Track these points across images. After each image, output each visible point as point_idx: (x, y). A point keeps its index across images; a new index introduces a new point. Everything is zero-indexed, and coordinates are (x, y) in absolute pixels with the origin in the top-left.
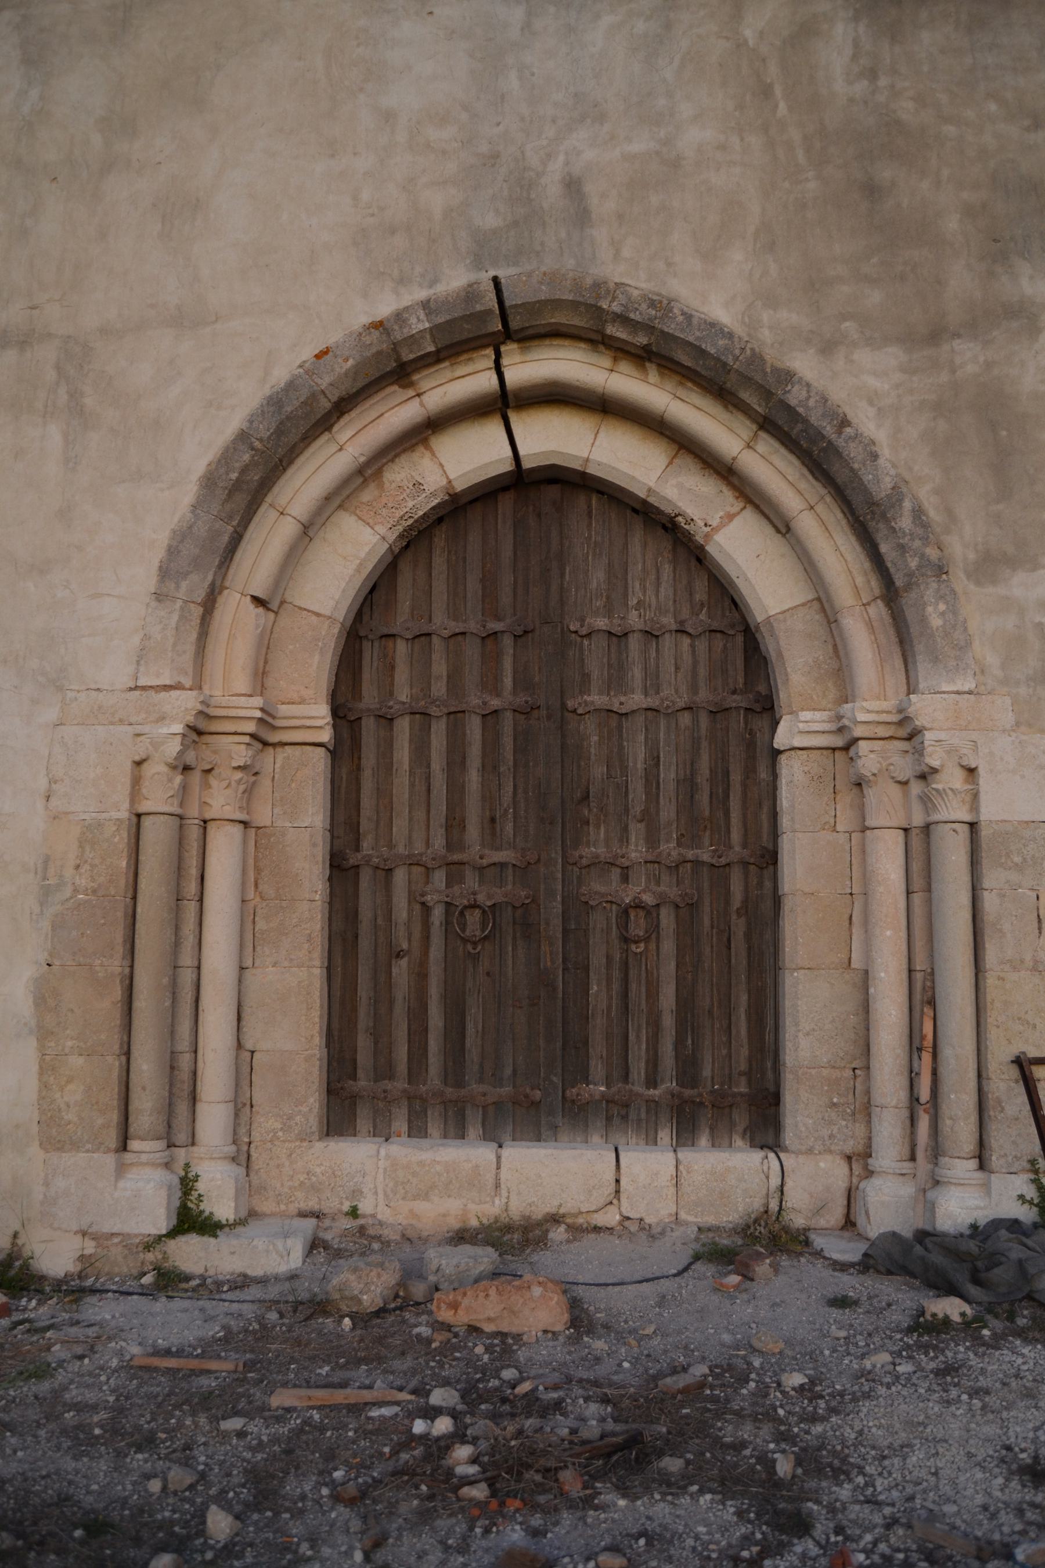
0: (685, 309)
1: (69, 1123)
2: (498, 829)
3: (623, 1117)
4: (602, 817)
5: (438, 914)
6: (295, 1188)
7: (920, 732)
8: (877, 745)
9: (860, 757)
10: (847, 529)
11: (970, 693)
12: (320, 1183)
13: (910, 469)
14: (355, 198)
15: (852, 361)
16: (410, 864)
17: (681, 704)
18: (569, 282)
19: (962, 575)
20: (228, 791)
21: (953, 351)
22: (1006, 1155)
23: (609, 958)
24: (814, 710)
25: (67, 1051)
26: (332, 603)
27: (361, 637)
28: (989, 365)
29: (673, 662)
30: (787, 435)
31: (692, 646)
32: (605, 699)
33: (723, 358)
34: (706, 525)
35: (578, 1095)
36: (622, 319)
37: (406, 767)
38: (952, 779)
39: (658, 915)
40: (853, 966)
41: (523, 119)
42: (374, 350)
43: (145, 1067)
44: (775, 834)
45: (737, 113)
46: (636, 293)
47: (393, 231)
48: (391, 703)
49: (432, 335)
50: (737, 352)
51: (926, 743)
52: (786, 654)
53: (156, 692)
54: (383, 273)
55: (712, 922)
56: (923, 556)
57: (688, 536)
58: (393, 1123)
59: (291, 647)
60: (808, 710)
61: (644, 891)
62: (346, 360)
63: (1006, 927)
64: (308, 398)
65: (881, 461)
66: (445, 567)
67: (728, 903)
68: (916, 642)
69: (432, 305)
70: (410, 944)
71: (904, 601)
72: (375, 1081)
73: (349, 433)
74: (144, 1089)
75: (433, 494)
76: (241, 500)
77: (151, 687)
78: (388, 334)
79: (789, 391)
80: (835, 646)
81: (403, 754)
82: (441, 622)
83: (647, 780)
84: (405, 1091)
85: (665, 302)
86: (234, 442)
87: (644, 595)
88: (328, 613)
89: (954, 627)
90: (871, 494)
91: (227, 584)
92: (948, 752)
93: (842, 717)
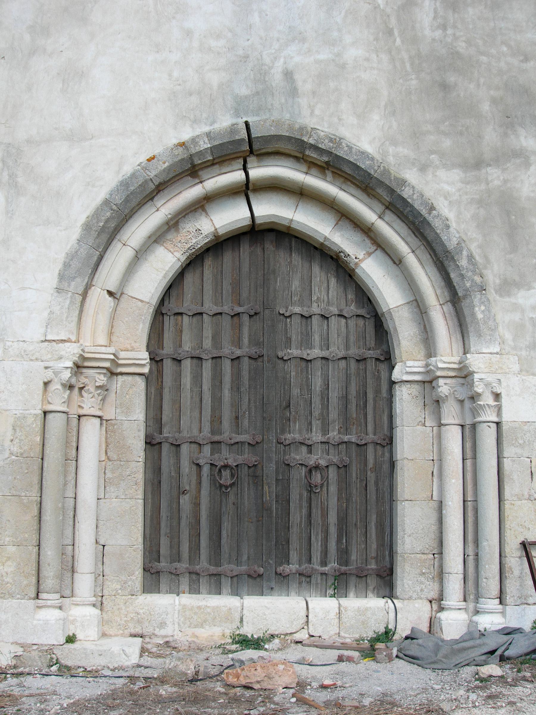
0: (348, 143)
1: (8, 583)
2: (240, 423)
3: (308, 582)
4: (297, 417)
5: (206, 470)
6: (128, 621)
7: (471, 374)
8: (448, 381)
9: (439, 387)
10: (432, 264)
11: (497, 353)
12: (142, 619)
13: (466, 234)
14: (170, 75)
15: (436, 176)
16: (190, 442)
17: (341, 355)
18: (286, 126)
19: (492, 291)
20: (93, 399)
21: (487, 173)
22: (514, 596)
23: (301, 496)
24: (414, 360)
25: (6, 543)
26: (150, 295)
27: (163, 314)
28: (505, 181)
29: (336, 332)
30: (402, 212)
31: (347, 323)
32: (299, 352)
33: (368, 171)
34: (356, 258)
35: (283, 570)
36: (315, 148)
37: (188, 387)
38: (488, 400)
39: (328, 471)
40: (434, 499)
41: (261, 38)
42: (180, 158)
43: (49, 553)
44: (391, 427)
45: (375, 42)
46: (322, 134)
47: (191, 94)
48: (180, 351)
49: (212, 152)
50: (376, 168)
51: (475, 380)
52: (399, 329)
53: (57, 343)
54: (185, 116)
55: (357, 475)
56: (473, 280)
57: (346, 263)
58: (180, 587)
59: (127, 319)
60: (410, 360)
61: (320, 458)
62: (164, 163)
63: (515, 477)
64: (143, 183)
65: (451, 229)
66: (211, 276)
67: (366, 465)
68: (469, 326)
69: (212, 135)
70: (190, 487)
71: (463, 304)
72: (171, 563)
73: (163, 202)
74: (49, 565)
75: (206, 236)
76: (105, 237)
77: (54, 341)
78: (188, 150)
79: (403, 190)
80: (425, 326)
81: (187, 380)
82: (209, 307)
83: (322, 397)
84: (187, 568)
85: (338, 139)
86: (101, 205)
87: (321, 295)
88: (147, 300)
89: (489, 318)
90: (446, 246)
91: (94, 283)
92: (486, 385)
93: (430, 365)
